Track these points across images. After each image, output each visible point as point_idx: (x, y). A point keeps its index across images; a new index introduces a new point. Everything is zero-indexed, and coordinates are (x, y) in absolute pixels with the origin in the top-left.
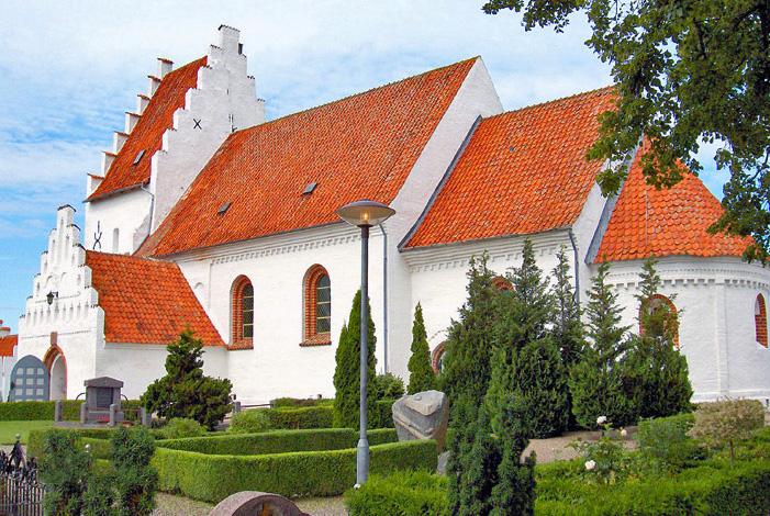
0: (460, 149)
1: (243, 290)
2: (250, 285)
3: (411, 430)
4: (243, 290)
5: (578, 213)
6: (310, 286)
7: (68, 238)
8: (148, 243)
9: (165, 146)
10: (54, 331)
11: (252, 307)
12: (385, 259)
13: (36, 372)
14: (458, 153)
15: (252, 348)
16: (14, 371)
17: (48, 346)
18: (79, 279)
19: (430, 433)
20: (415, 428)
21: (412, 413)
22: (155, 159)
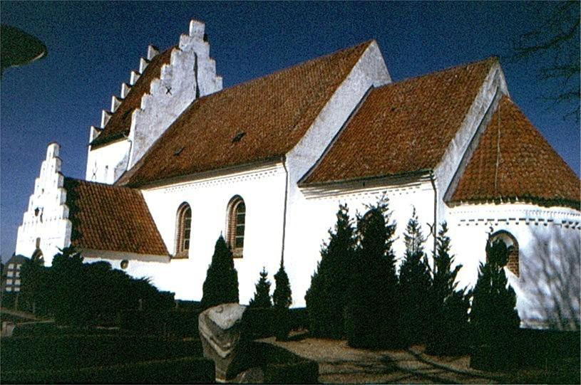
0: (355, 110)
1: (185, 211)
2: (243, 204)
3: (212, 342)
4: (185, 211)
5: (439, 159)
6: (233, 206)
7: (52, 166)
8: (125, 176)
9: (143, 106)
10: (37, 237)
11: (190, 227)
12: (286, 192)
13: (11, 270)
14: (352, 113)
15: (188, 258)
16: (513, 238)
17: (34, 249)
18: (57, 198)
19: (228, 348)
20: (215, 342)
21: (212, 324)
22: (135, 114)
